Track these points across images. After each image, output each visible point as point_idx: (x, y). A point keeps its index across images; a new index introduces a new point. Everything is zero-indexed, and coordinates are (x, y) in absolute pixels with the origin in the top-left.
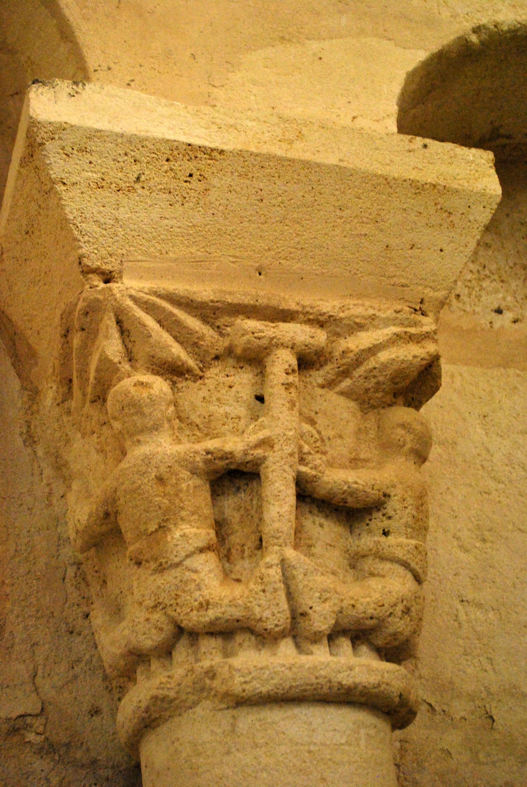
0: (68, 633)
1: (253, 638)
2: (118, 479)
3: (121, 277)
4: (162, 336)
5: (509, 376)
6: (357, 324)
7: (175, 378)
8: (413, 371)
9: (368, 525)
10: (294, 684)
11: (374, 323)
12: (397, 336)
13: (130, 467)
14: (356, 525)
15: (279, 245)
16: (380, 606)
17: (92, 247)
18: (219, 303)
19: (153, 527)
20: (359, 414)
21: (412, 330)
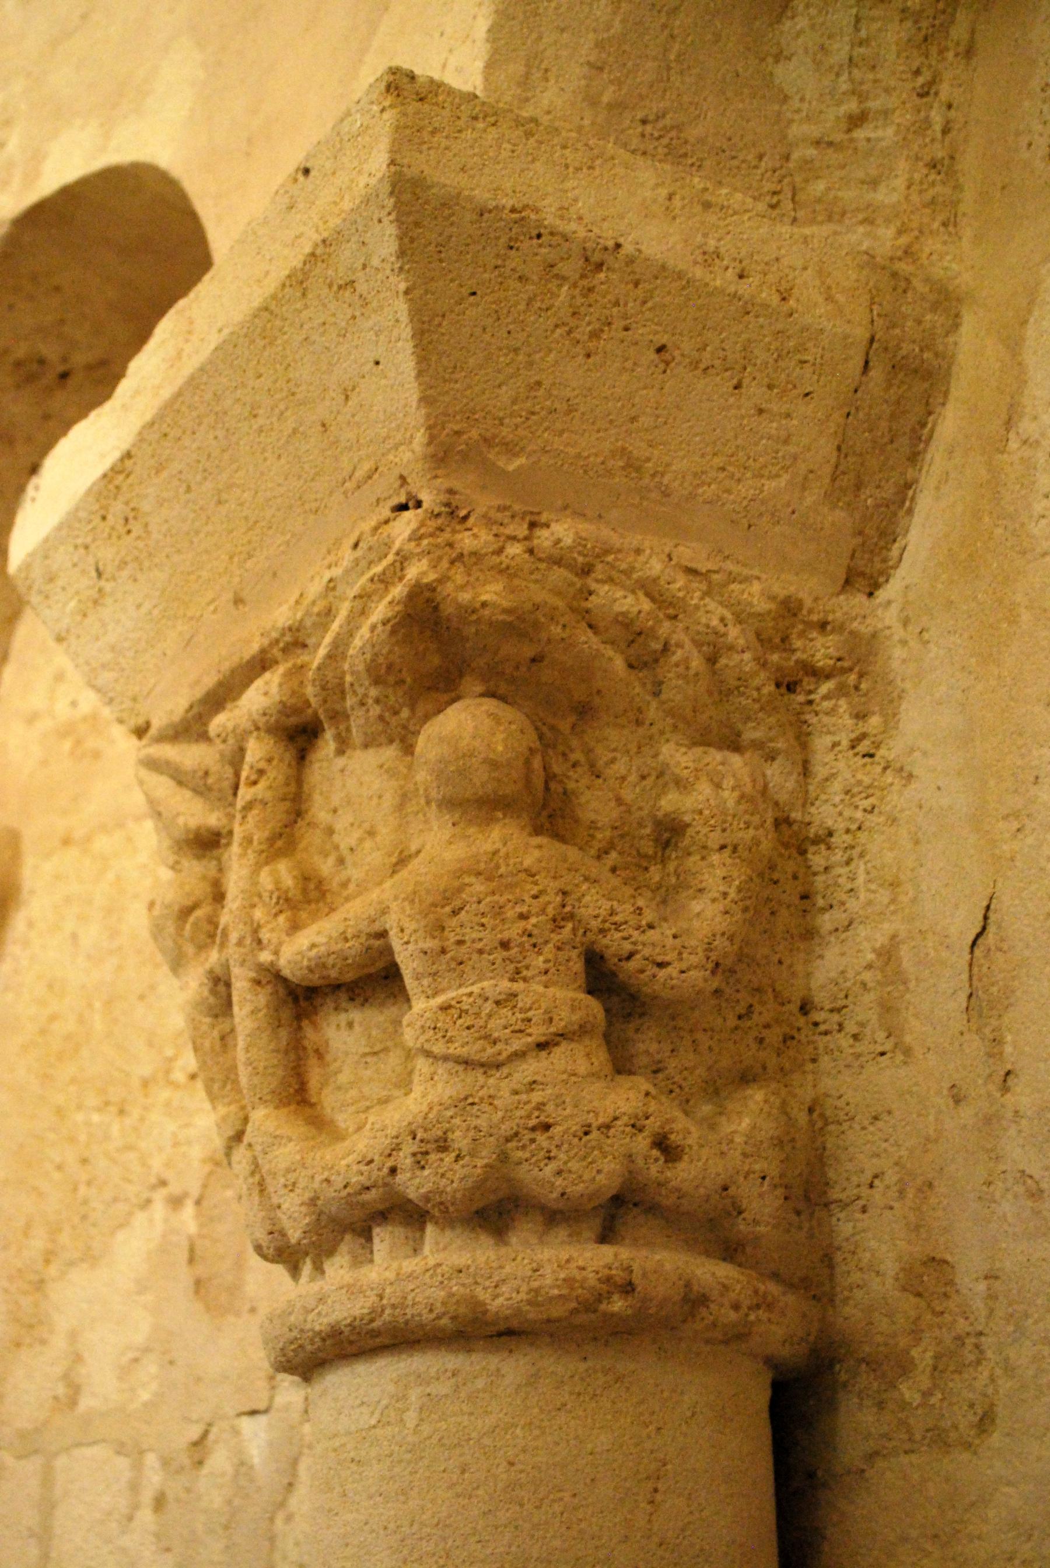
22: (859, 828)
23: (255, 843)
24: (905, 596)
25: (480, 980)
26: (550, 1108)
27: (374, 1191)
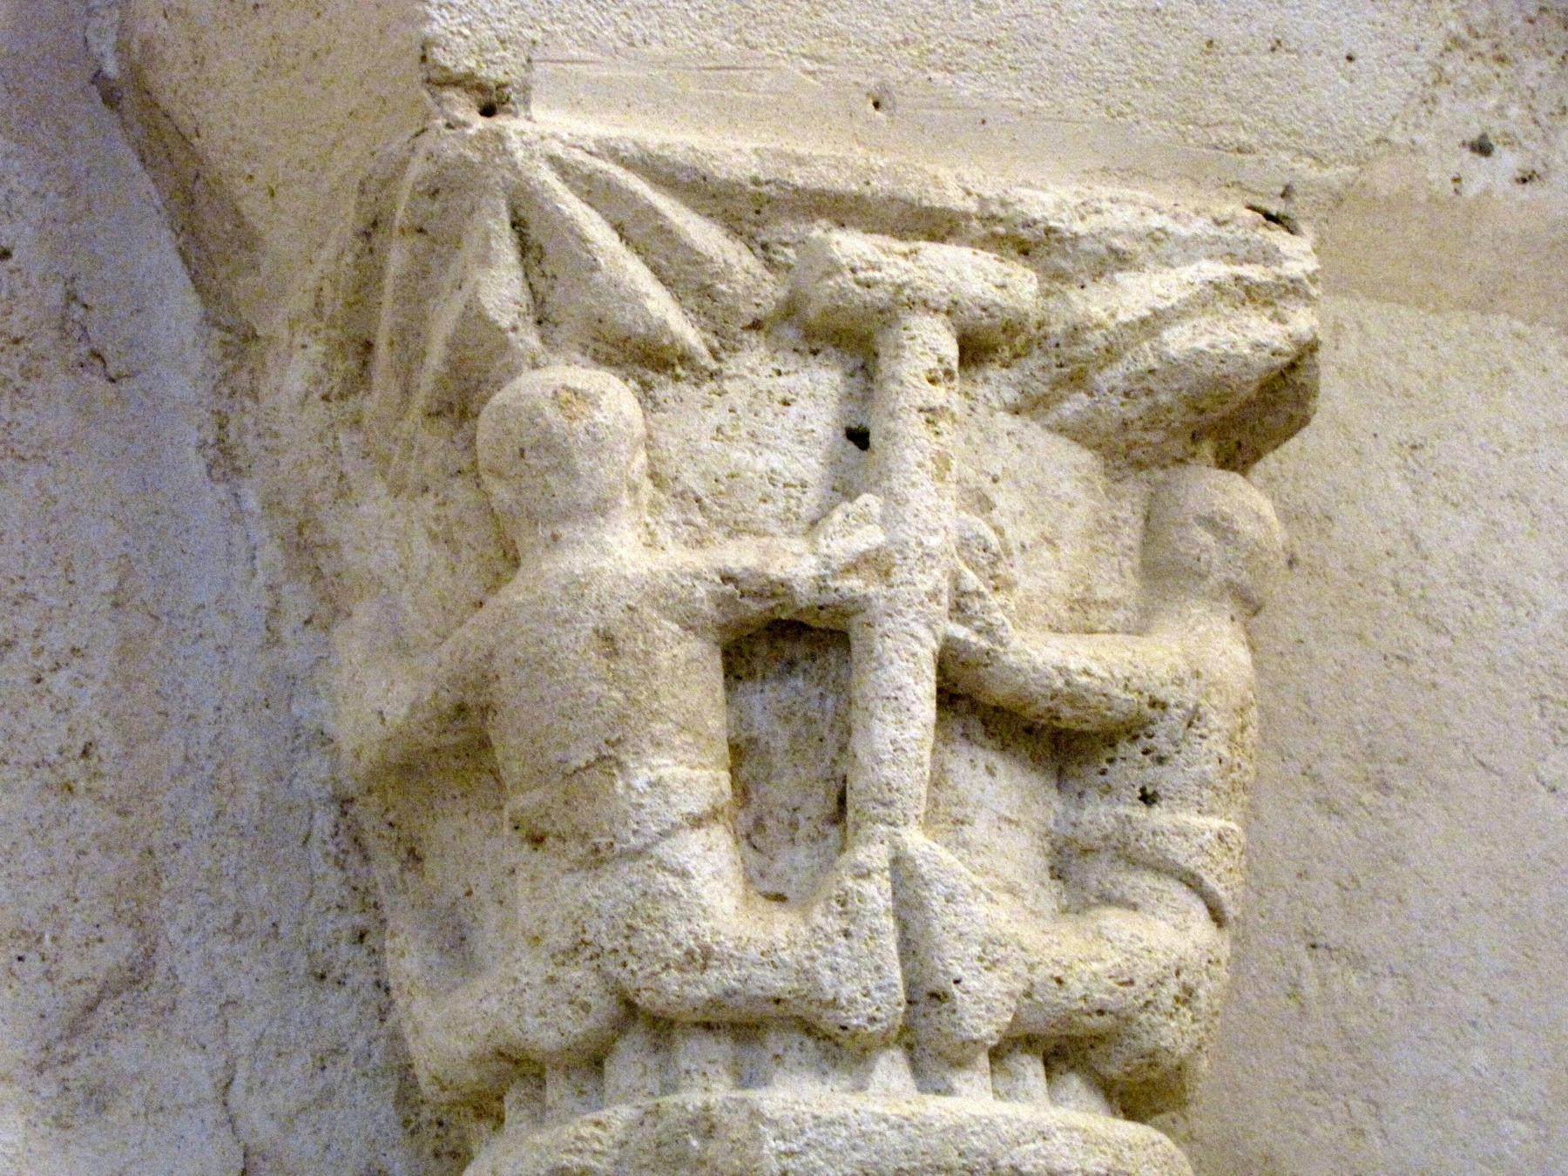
0: (312, 979)
1: (810, 1043)
2: (495, 631)
3: (526, 103)
4: (624, 268)
5: (1491, 336)
6: (1113, 251)
7: (650, 375)
8: (1248, 383)
9: (1103, 772)
10: (905, 1165)
11: (1158, 251)
12: (1217, 287)
13: (532, 603)
14: (1074, 769)
15: (932, 31)
16: (1122, 984)
17: (458, 20)
18: (772, 186)
19: (582, 756)
20: (1100, 483)
21: (1255, 273)
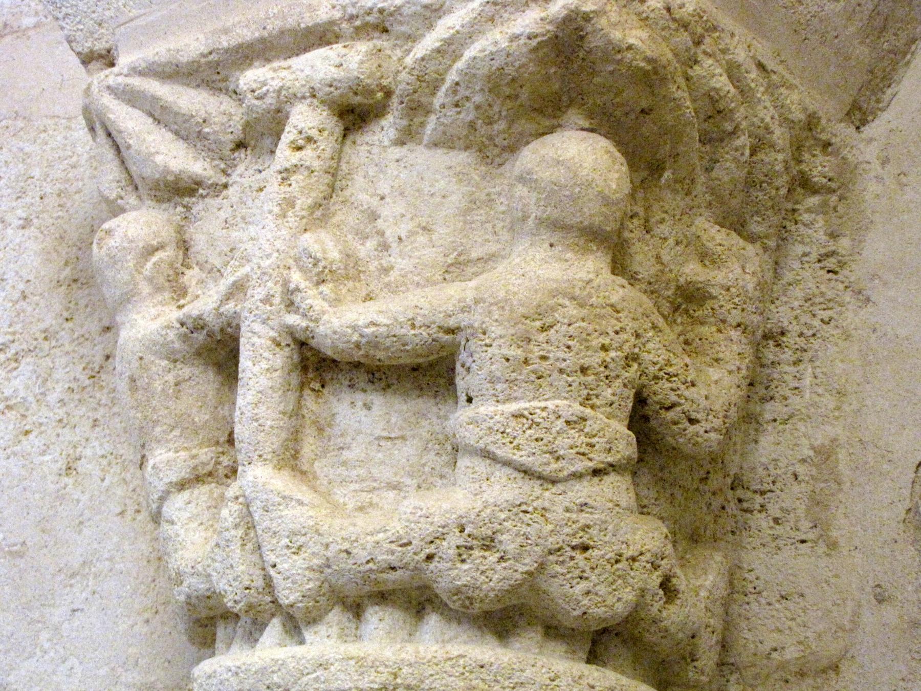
18: (214, 54)
22: (814, 335)
23: (297, 207)
24: (888, 137)
25: (554, 398)
26: (594, 532)
27: (399, 573)
